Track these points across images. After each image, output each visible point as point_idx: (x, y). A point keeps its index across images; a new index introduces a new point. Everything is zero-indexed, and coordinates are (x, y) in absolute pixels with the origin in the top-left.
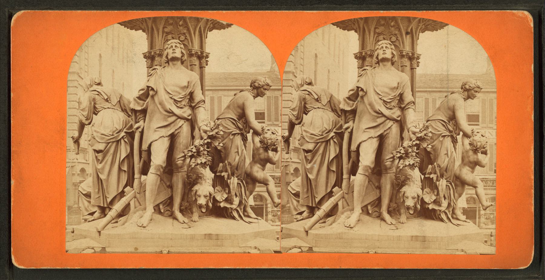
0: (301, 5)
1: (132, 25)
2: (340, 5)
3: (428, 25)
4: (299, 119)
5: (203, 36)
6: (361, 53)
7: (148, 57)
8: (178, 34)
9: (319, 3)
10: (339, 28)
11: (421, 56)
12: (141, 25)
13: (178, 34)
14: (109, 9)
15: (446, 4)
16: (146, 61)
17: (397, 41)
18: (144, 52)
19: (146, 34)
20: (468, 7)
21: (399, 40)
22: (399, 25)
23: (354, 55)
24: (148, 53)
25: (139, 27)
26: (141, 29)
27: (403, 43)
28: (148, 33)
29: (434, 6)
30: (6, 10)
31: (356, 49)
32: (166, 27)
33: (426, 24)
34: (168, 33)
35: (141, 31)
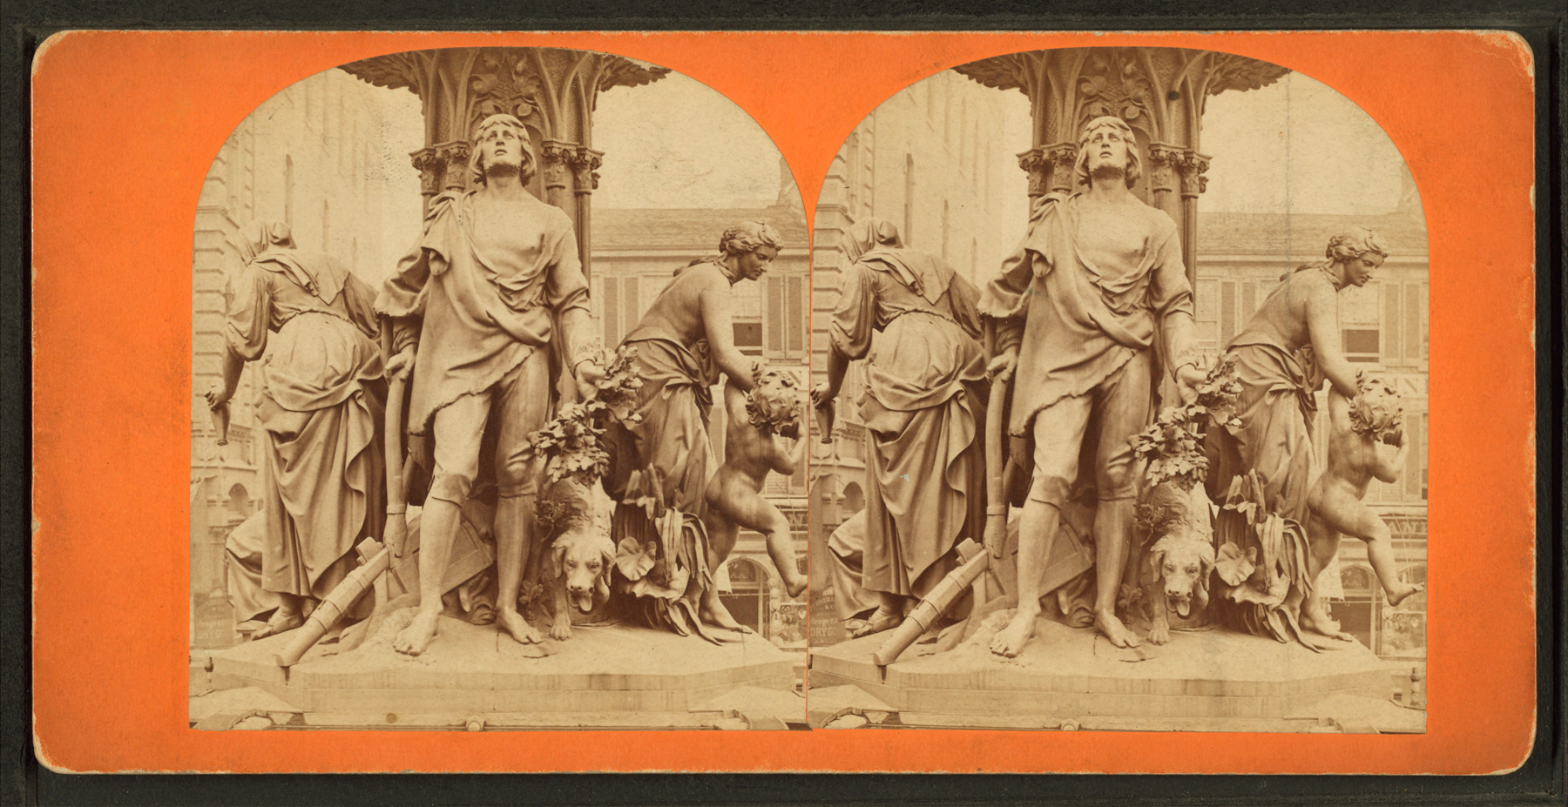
0: (866, 14)
1: (379, 72)
3: (1232, 72)
4: (862, 344)
5: (585, 105)
6: (1038, 153)
7: (1034, 167)
9: (918, 8)
11: (1211, 161)
12: (405, 73)
14: (313, 26)
15: (1284, 11)
16: (420, 177)
17: (1143, 119)
18: (414, 150)
19: (421, 98)
20: (1347, 20)
22: (1147, 74)
23: (410, 158)
24: (426, 152)
25: (401, 76)
29: (1249, 17)
30: (19, 28)
31: (418, 139)
32: (478, 79)
33: (1226, 70)
34: (484, 95)
35: (407, 88)
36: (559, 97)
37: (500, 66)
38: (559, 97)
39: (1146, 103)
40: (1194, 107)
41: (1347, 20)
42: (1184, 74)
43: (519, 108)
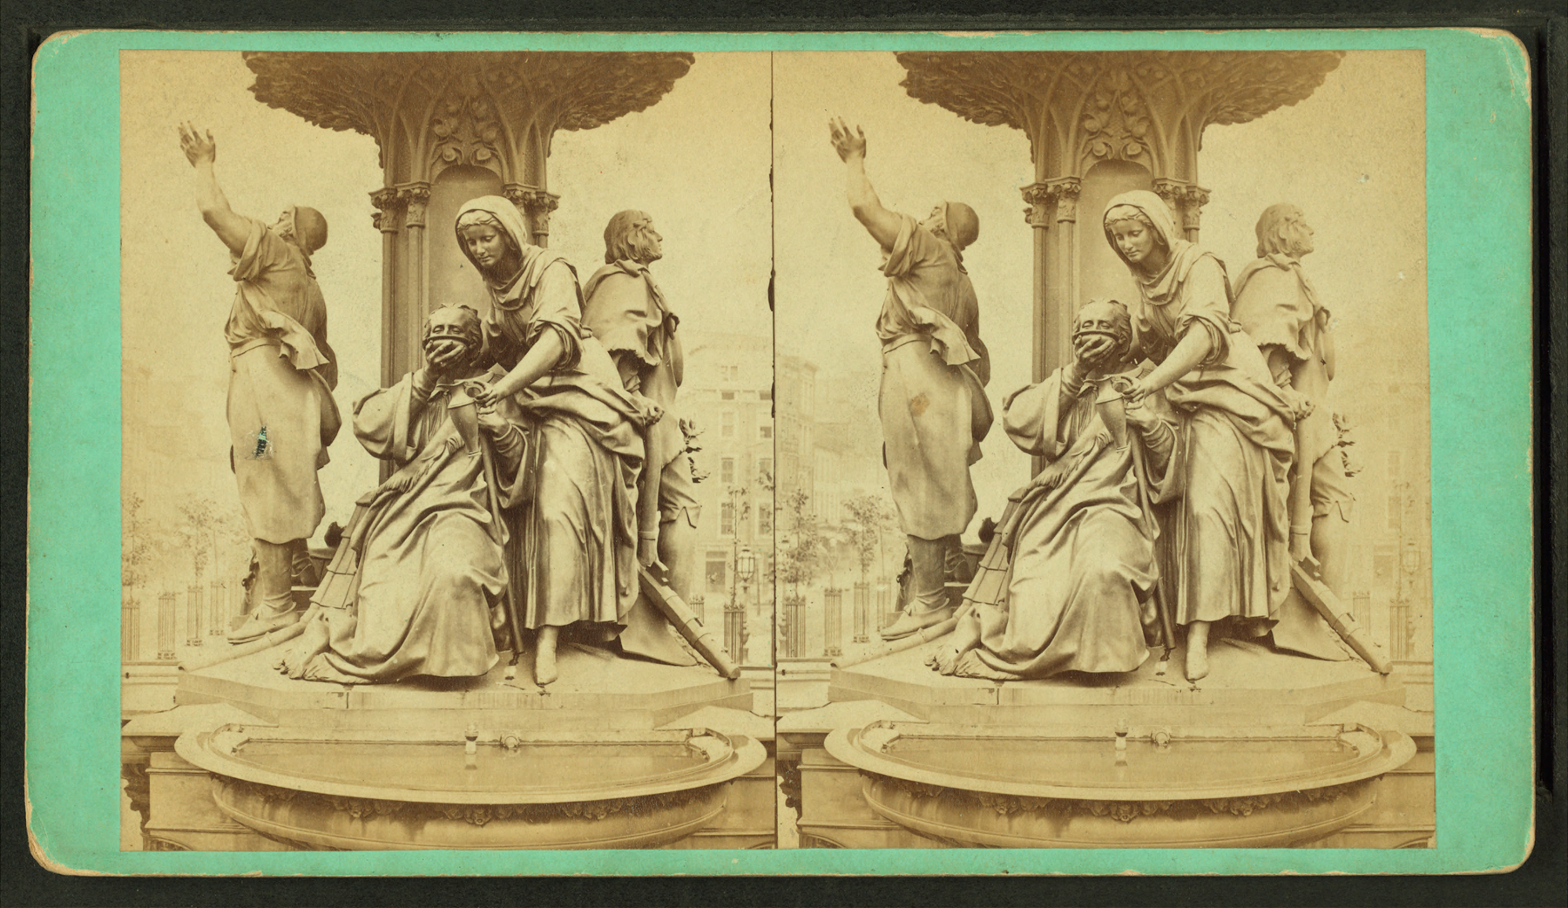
0: (862, 14)
2: (973, 13)
5: (541, 149)
6: (390, 190)
8: (1122, 139)
9: (914, 8)
10: (310, 123)
13: (1122, 139)
17: (495, 160)
19: (1029, 136)
21: (1148, 152)
23: (1021, 192)
26: (1233, 121)
27: (1160, 155)
28: (1037, 137)
29: (1241, 17)
32: (440, 122)
34: (444, 138)
36: (518, 145)
37: (1111, 106)
38: (518, 145)
39: (497, 146)
40: (1191, 136)
41: (1337, 20)
42: (532, 121)
43: (1128, 148)
